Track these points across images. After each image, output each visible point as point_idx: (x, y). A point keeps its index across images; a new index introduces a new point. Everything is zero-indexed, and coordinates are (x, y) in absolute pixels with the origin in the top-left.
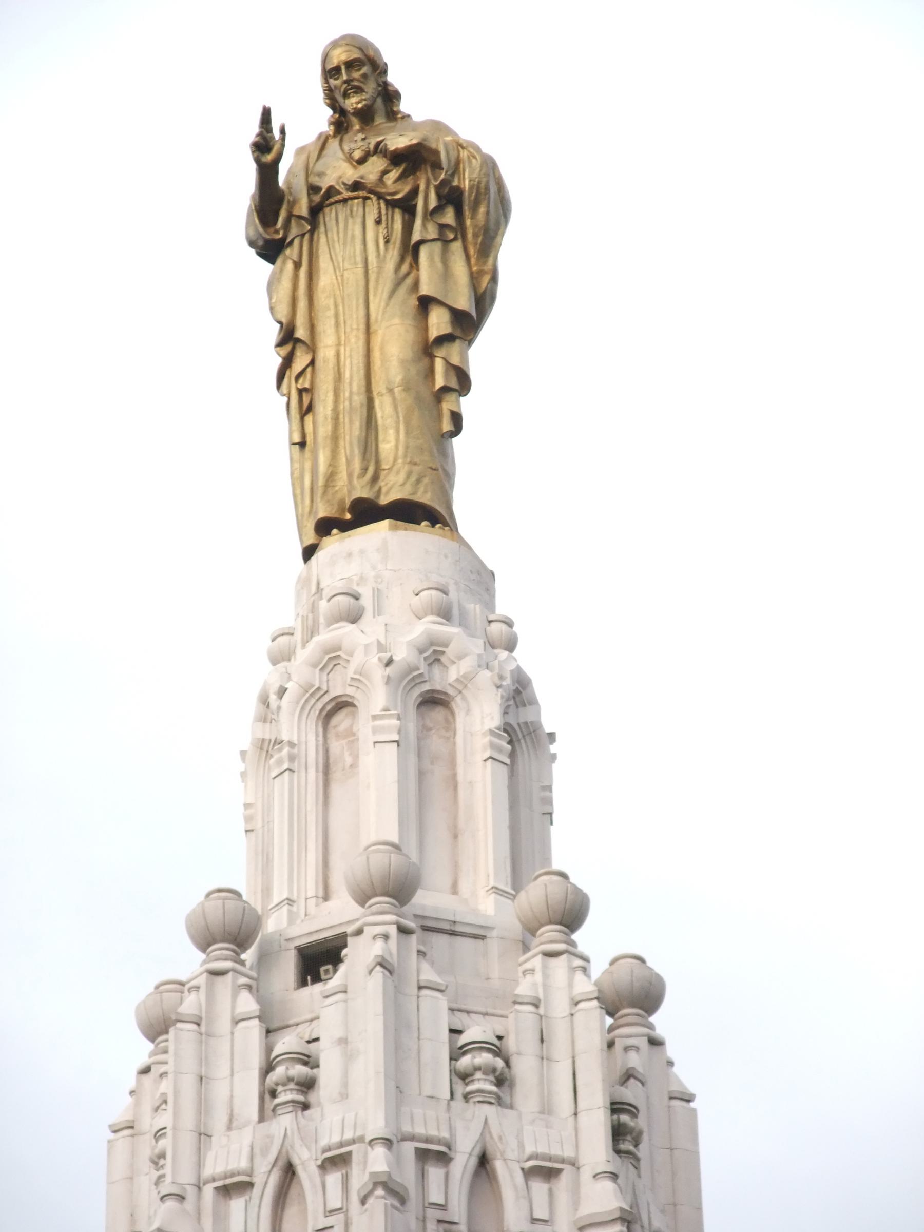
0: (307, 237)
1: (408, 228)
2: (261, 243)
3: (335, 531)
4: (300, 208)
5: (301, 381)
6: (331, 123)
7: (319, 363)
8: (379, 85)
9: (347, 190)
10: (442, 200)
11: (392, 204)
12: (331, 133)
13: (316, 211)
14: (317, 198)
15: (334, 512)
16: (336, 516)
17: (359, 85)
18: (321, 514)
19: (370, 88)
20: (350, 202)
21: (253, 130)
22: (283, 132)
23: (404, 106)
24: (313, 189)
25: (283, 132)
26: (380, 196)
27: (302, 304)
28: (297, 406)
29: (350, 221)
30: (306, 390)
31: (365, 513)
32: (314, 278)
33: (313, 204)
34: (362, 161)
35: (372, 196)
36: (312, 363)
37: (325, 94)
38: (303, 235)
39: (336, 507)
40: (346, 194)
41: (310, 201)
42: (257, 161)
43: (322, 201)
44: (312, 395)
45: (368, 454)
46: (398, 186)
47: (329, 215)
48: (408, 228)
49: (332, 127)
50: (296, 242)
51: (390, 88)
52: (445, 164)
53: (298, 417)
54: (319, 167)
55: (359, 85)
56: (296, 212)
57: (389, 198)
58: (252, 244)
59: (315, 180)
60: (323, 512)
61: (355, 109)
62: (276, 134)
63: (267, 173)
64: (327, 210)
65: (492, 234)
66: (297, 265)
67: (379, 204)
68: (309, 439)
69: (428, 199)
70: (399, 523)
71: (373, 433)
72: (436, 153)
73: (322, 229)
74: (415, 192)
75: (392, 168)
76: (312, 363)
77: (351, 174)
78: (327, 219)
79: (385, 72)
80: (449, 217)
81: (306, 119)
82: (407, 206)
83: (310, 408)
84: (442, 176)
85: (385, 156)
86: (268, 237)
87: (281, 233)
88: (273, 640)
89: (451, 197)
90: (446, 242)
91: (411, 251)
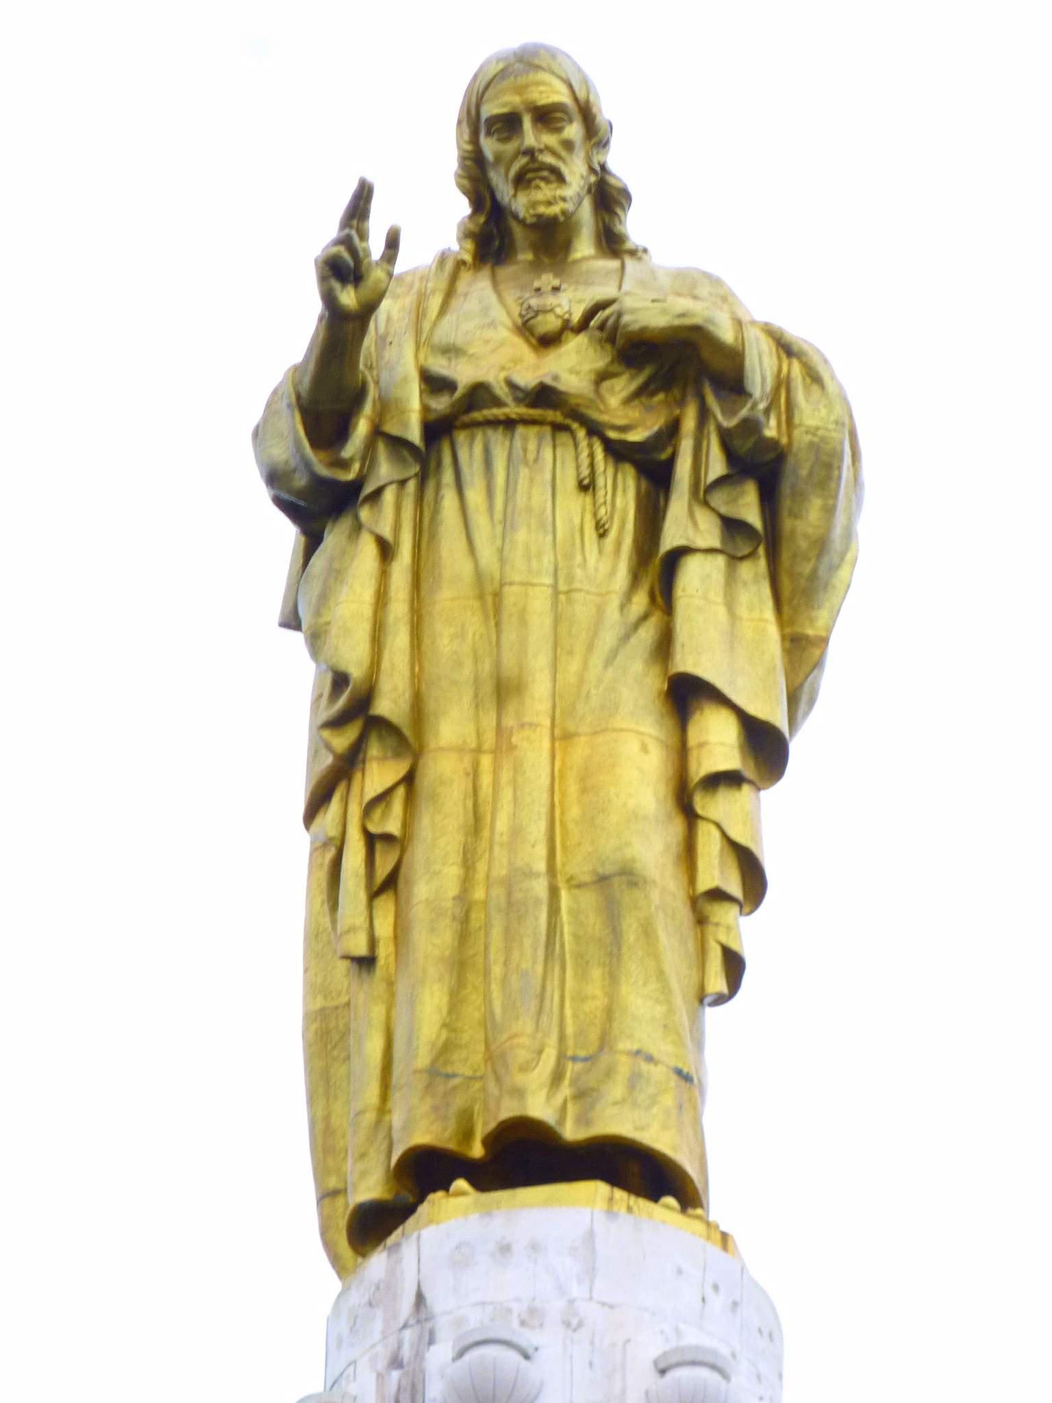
0: (411, 486)
1: (651, 517)
2: (300, 481)
3: (461, 1184)
4: (405, 425)
5: (377, 813)
6: (467, 235)
7: (426, 780)
8: (592, 170)
9: (518, 401)
10: (717, 443)
11: (618, 452)
12: (468, 258)
13: (438, 430)
14: (441, 404)
15: (447, 1135)
16: (452, 1146)
17: (530, 173)
18: (423, 1137)
19: (576, 173)
20: (520, 430)
21: (324, 232)
22: (393, 243)
23: (635, 225)
24: (434, 383)
25: (393, 243)
26: (594, 430)
27: (399, 640)
28: (362, 870)
29: (524, 472)
30: (388, 838)
31: (425, 1172)
32: (425, 586)
33: (432, 417)
34: (547, 342)
35: (575, 426)
36: (409, 779)
37: (463, 166)
38: (402, 483)
39: (452, 1125)
40: (513, 410)
41: (425, 409)
42: (329, 300)
43: (460, 413)
44: (403, 851)
45: (545, 1018)
46: (634, 413)
47: (469, 450)
48: (651, 517)
49: (469, 245)
50: (389, 496)
51: (612, 181)
52: (757, 392)
53: (363, 896)
54: (447, 331)
55: (530, 173)
56: (392, 428)
57: (612, 435)
58: (274, 478)
59: (439, 366)
60: (423, 1130)
61: (539, 216)
62: (376, 246)
63: (342, 333)
64: (461, 437)
65: (836, 560)
66: (386, 550)
67: (590, 446)
68: (385, 952)
69: (698, 458)
70: (391, 1240)
71: (557, 969)
72: (735, 357)
73: (448, 476)
74: (672, 431)
75: (616, 368)
76: (409, 779)
77: (531, 369)
78: (463, 454)
79: (604, 144)
80: (749, 509)
81: (428, 218)
82: (652, 468)
83: (391, 882)
84: (744, 412)
85: (611, 340)
86: (323, 471)
87: (356, 466)
88: (461, 1354)
89: (761, 465)
90: (734, 559)
91: (659, 571)
